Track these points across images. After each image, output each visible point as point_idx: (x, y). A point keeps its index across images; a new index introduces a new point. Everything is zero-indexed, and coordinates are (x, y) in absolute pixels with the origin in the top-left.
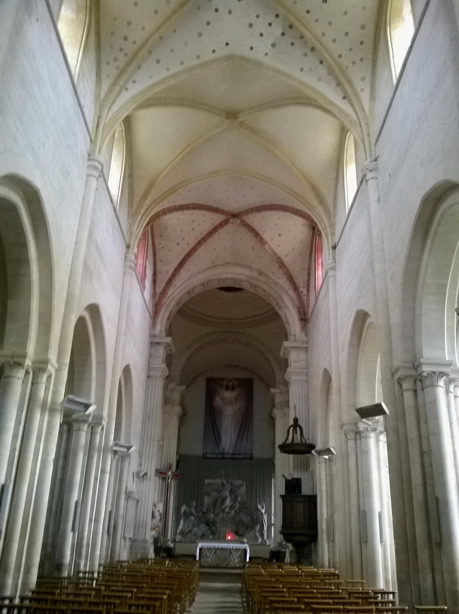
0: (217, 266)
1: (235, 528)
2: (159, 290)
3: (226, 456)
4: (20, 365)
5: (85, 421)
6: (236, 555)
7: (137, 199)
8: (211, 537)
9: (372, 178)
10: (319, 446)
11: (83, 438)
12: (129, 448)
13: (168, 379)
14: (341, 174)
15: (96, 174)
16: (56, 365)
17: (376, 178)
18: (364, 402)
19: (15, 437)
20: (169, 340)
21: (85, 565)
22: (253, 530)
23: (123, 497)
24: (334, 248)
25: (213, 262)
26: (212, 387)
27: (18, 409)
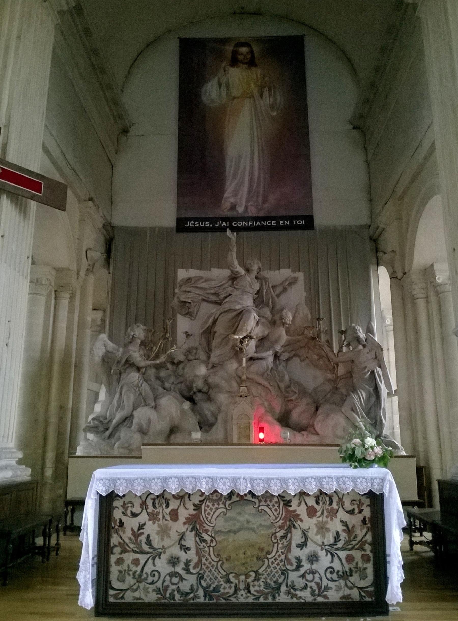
1: (278, 407)
8: (197, 435)
22: (346, 408)
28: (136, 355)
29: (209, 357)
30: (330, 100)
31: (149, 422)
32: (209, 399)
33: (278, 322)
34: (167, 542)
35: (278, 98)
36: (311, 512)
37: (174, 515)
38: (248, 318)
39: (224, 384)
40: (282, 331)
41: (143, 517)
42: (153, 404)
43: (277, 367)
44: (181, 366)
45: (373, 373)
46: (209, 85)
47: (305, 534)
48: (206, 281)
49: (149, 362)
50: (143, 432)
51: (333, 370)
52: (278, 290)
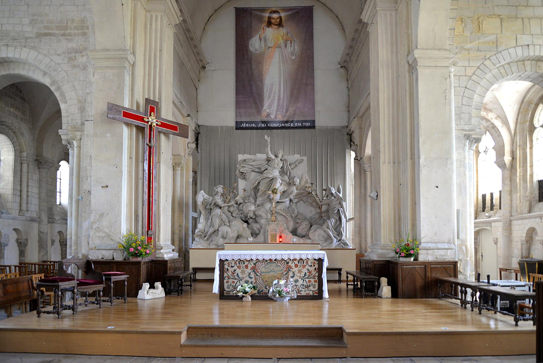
1: (291, 225)
6: (300, 271)
8: (251, 239)
22: (325, 227)
28: (219, 200)
29: (256, 201)
30: (328, 42)
31: (227, 233)
32: (256, 222)
33: (292, 184)
34: (244, 276)
35: (296, 47)
36: (296, 266)
37: (247, 267)
38: (276, 183)
39: (263, 215)
40: (294, 188)
41: (236, 267)
42: (228, 224)
43: (291, 206)
44: (241, 205)
45: (339, 210)
46: (254, 39)
47: (293, 273)
48: (254, 161)
49: (226, 205)
50: (224, 238)
51: (320, 208)
52: (292, 166)
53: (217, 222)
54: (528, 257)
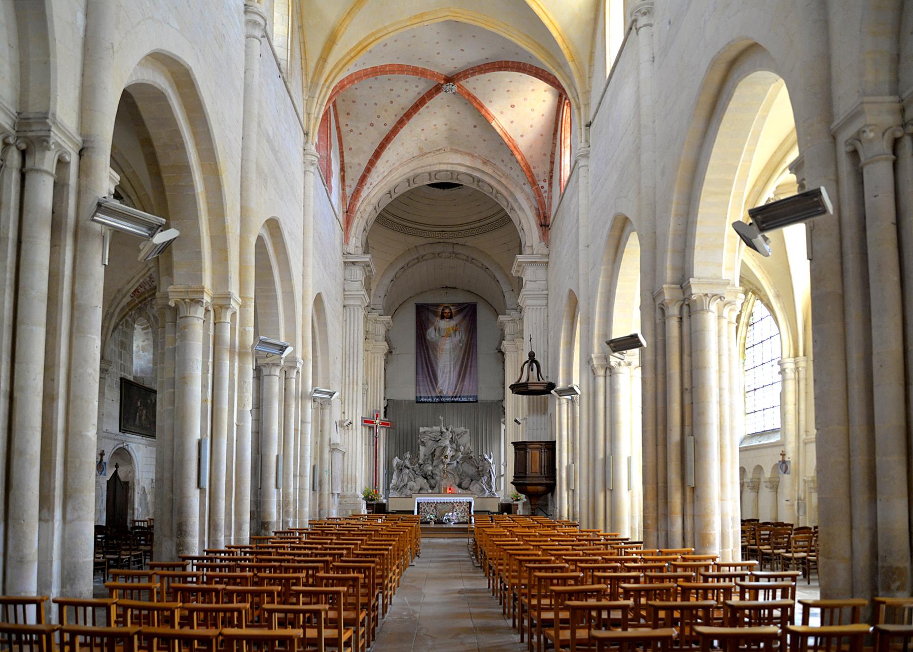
0: (426, 154)
1: (458, 481)
2: (349, 191)
3: (444, 400)
4: (199, 302)
5: (277, 365)
7: (312, 64)
8: (430, 491)
9: (645, 26)
10: (561, 385)
11: (276, 385)
12: (332, 394)
13: (370, 309)
14: (602, 12)
15: (258, 33)
16: (240, 300)
17: (651, 25)
18: (619, 331)
19: (204, 386)
20: (367, 258)
21: (294, 522)
23: (327, 449)
24: (589, 125)
25: (421, 149)
26: (424, 315)
27: (203, 354)
28: (408, 464)
50: (411, 490)
53: (406, 479)
54: (776, 518)
